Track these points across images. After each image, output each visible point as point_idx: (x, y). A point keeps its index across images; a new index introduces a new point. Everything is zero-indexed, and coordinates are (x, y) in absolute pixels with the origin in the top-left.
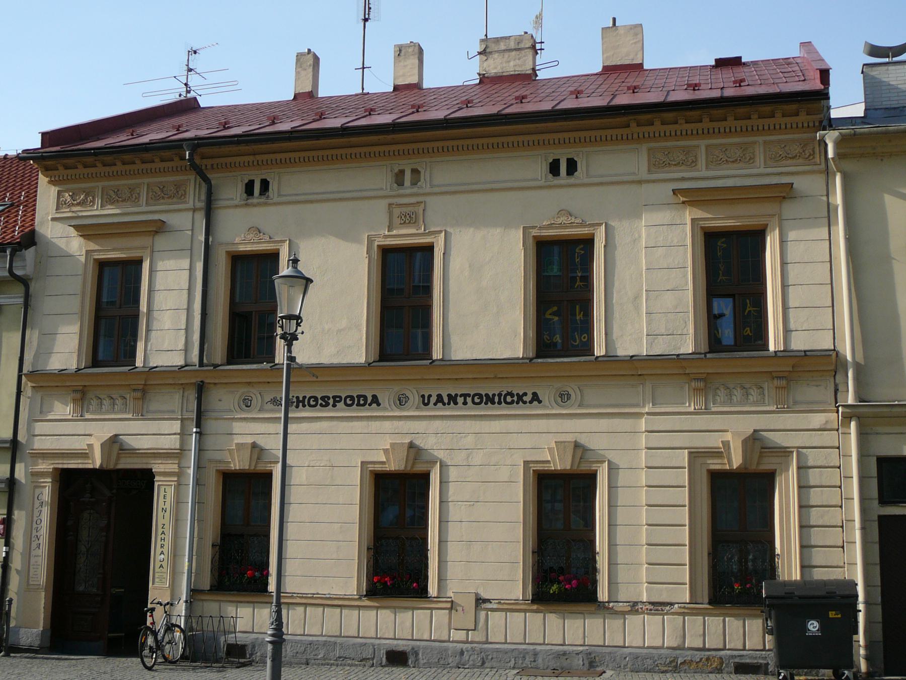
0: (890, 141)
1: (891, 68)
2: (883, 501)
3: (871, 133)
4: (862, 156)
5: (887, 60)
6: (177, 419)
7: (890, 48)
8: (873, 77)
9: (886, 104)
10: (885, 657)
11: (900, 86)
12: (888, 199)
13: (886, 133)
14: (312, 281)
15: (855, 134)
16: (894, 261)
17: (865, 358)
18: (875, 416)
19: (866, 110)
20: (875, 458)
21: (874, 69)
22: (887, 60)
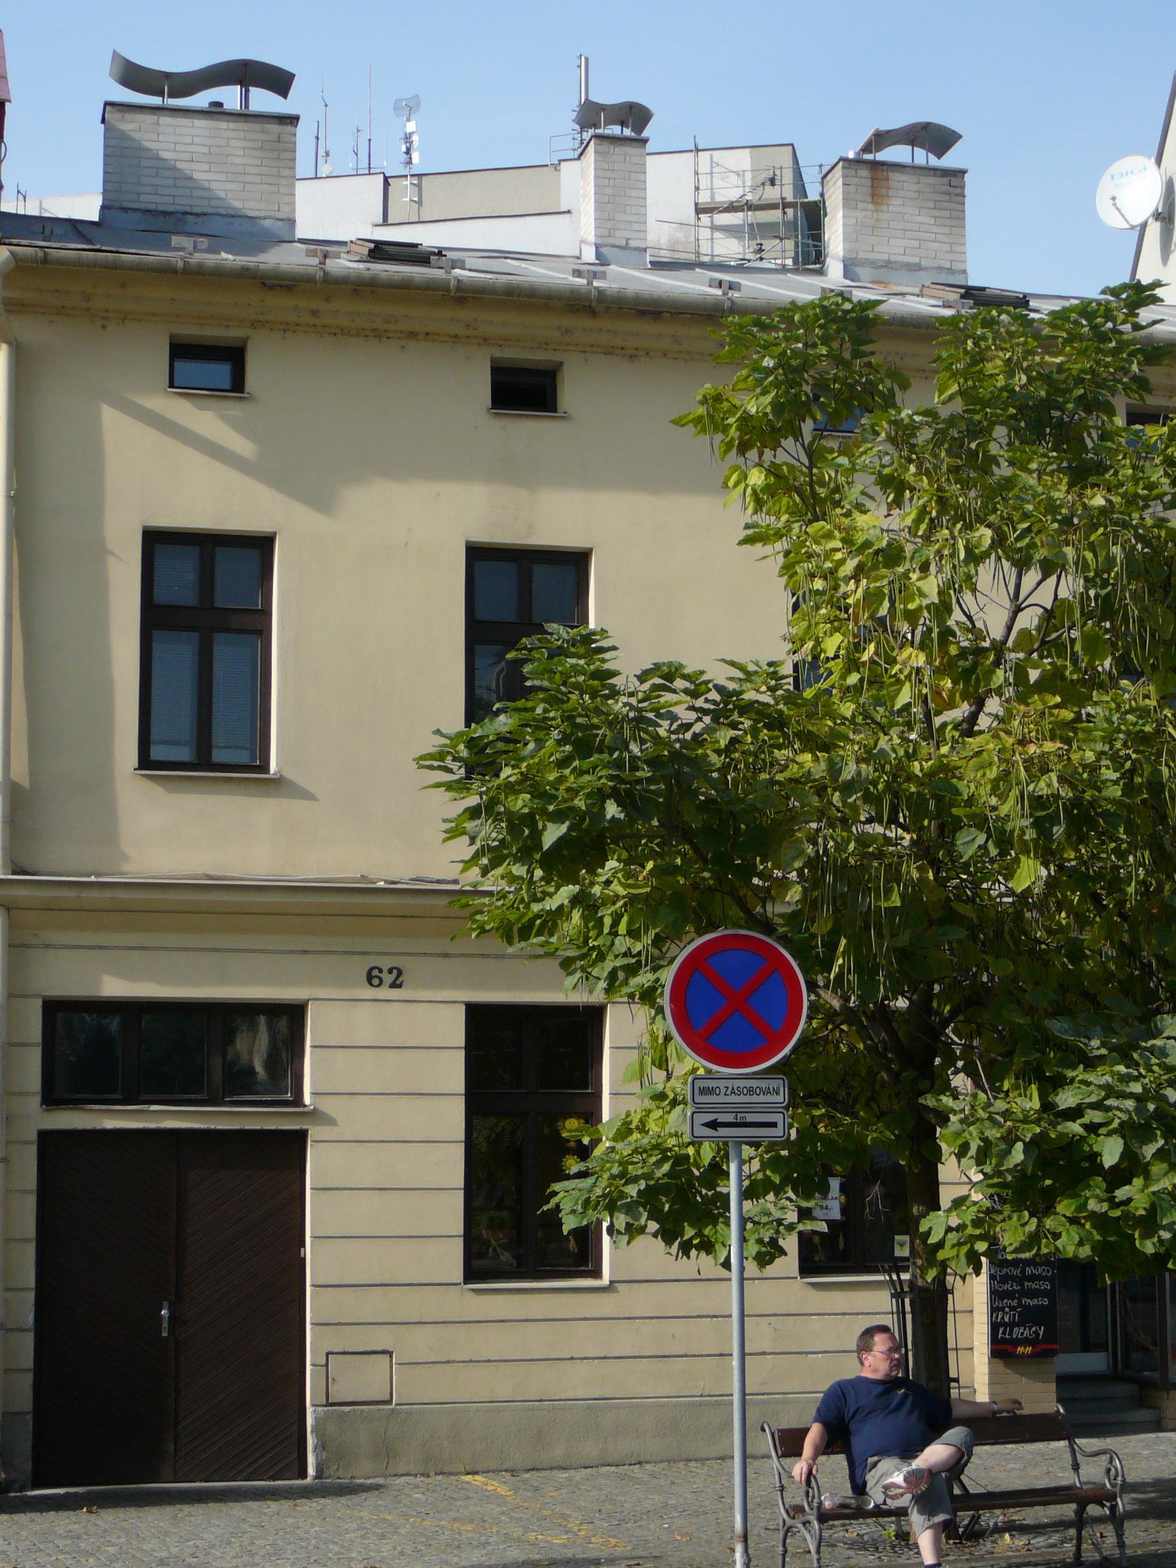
0: (123, 286)
1: (165, 120)
2: (52, 1098)
3: (80, 263)
4: (62, 312)
5: (156, 101)
6: (246, 749)
7: (168, 76)
8: (123, 136)
9: (149, 201)
10: (36, 1447)
11: (179, 165)
12: (110, 416)
13: (115, 267)
14: (963, 172)
15: (45, 260)
16: (111, 560)
17: (33, 773)
18: (49, 907)
19: (103, 207)
20: (39, 1003)
21: (129, 116)
22: (156, 101)
